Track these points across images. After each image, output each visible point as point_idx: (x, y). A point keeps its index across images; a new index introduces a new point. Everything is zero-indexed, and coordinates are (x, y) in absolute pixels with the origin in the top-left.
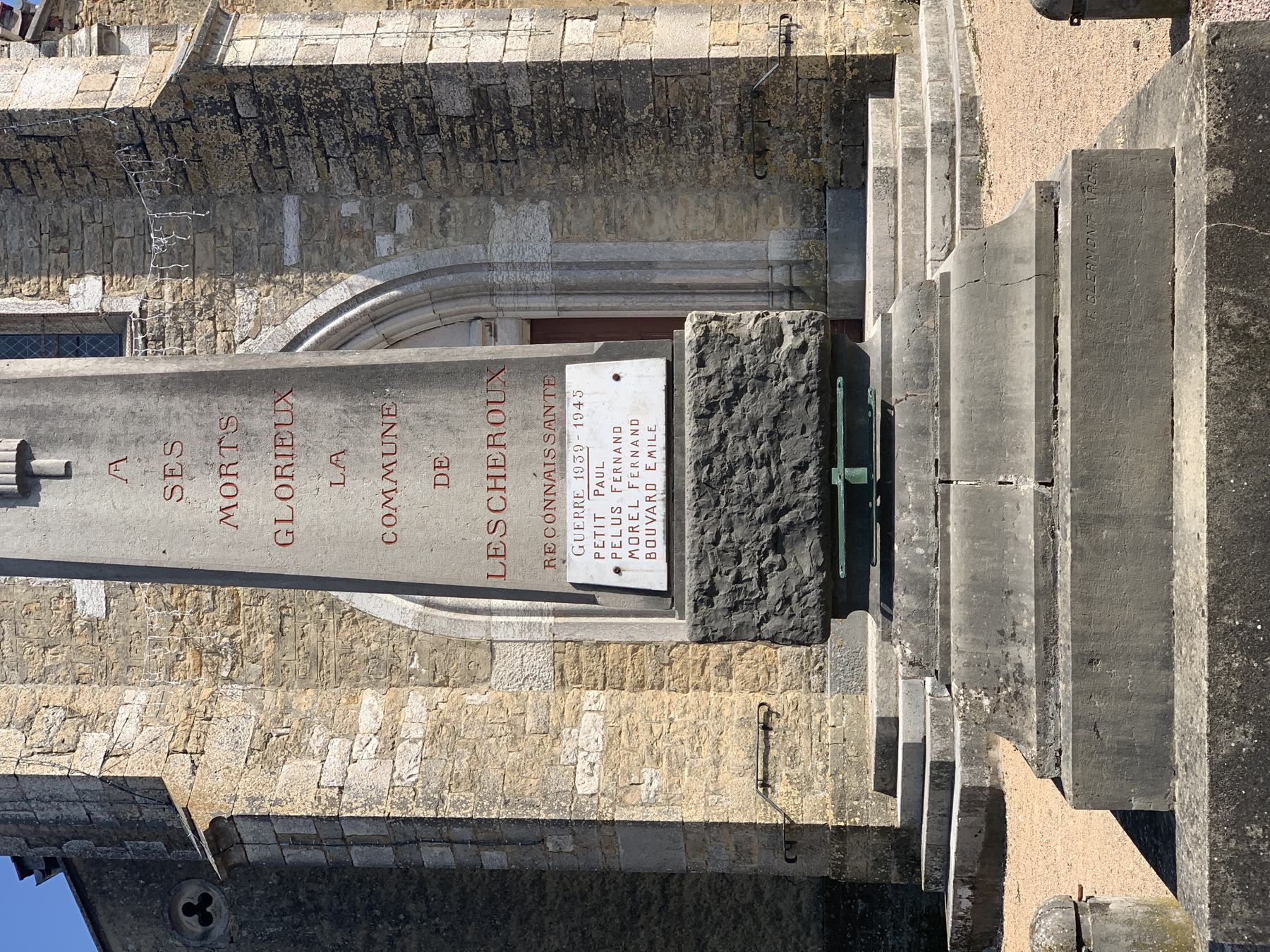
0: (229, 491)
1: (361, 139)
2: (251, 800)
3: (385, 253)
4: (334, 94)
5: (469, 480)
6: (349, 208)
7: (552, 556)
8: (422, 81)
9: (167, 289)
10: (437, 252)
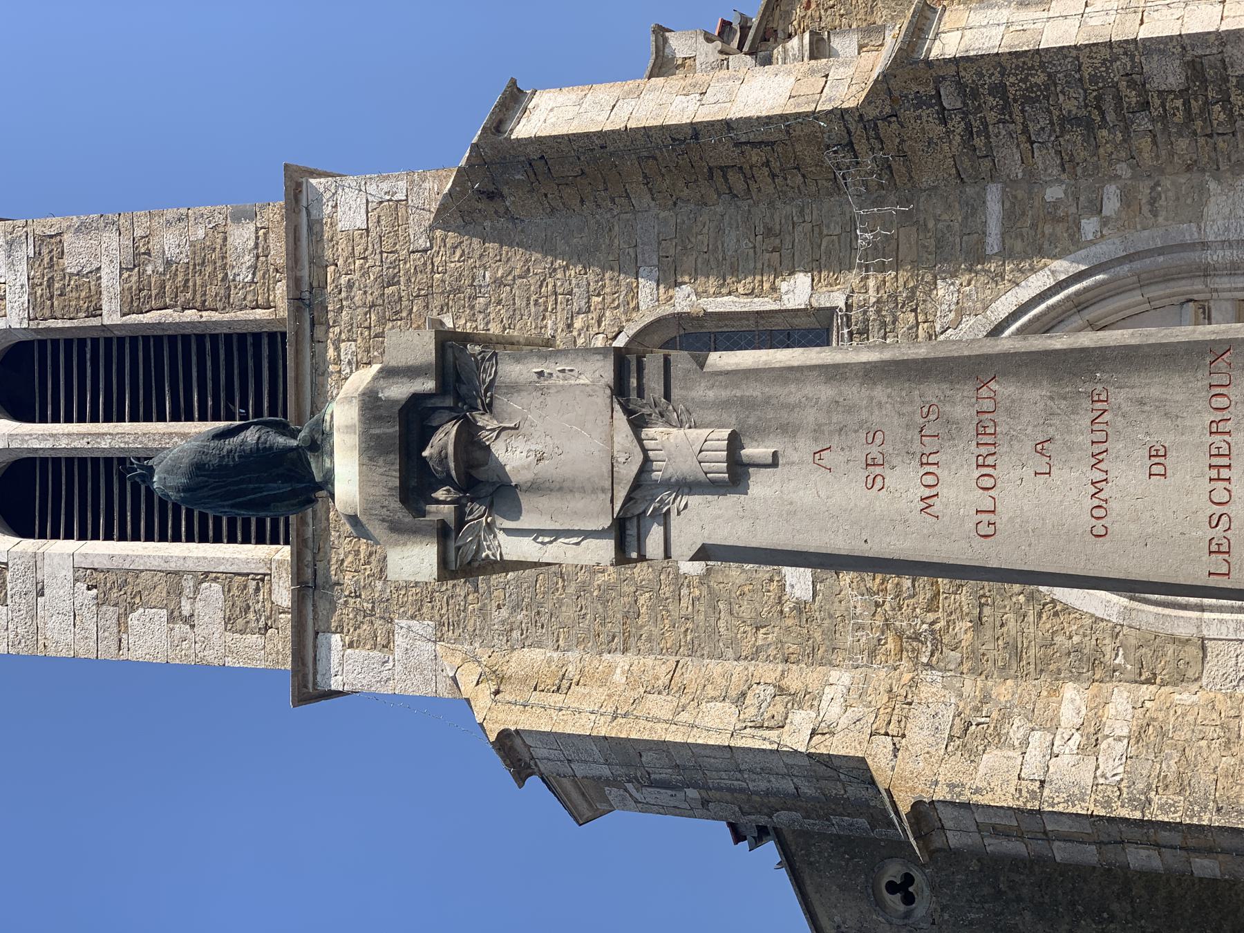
0: (930, 480)
1: (1067, 121)
2: (952, 786)
3: (1090, 237)
4: (1040, 79)
5: (1188, 476)
6: (1054, 193)
8: (1132, 57)
9: (871, 283)
10: (1146, 233)
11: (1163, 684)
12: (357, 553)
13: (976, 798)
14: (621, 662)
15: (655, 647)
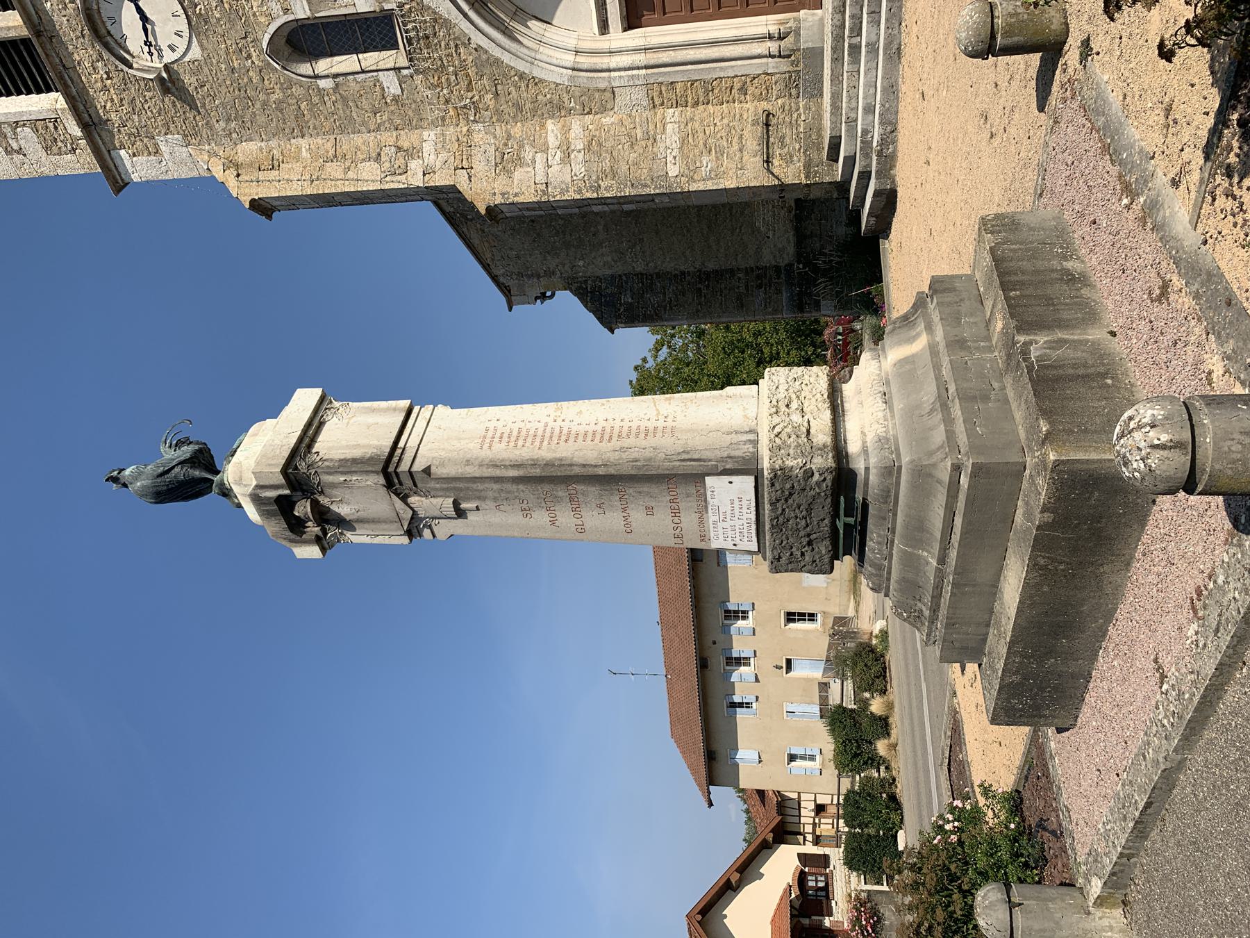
2: (503, 194)
11: (596, 113)
12: (112, 100)
13: (516, 199)
14: (304, 143)
15: (319, 131)
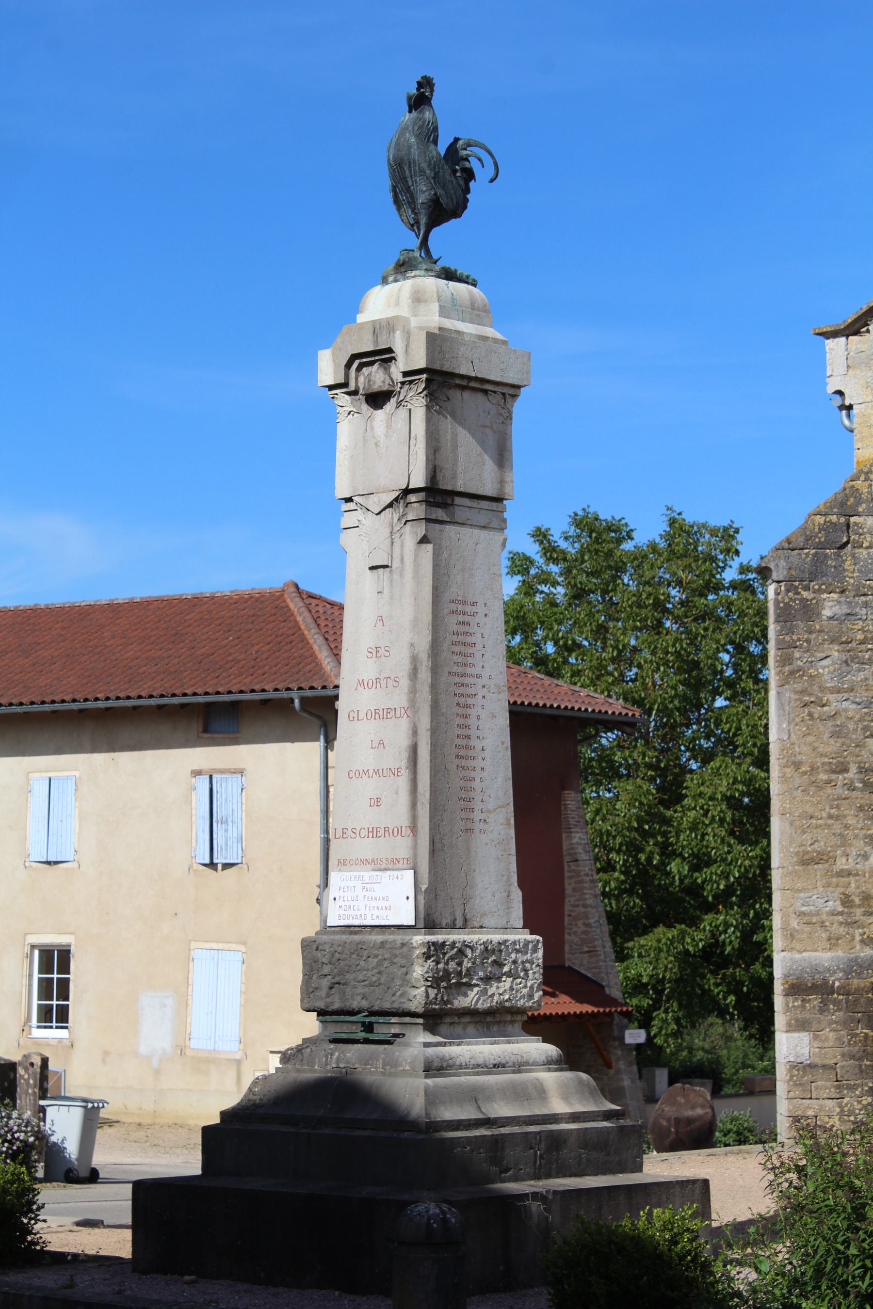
0: (370, 684)
7: (343, 863)
